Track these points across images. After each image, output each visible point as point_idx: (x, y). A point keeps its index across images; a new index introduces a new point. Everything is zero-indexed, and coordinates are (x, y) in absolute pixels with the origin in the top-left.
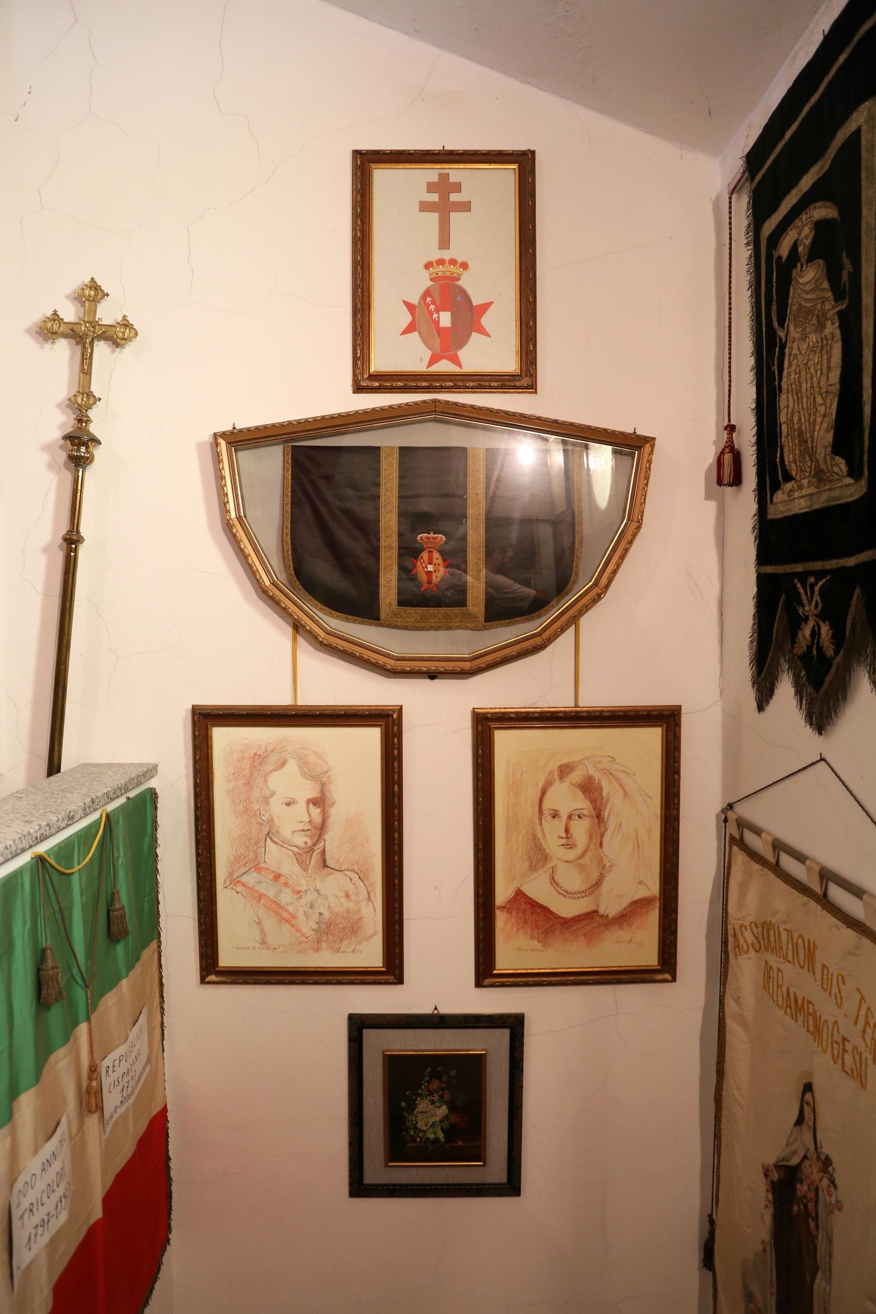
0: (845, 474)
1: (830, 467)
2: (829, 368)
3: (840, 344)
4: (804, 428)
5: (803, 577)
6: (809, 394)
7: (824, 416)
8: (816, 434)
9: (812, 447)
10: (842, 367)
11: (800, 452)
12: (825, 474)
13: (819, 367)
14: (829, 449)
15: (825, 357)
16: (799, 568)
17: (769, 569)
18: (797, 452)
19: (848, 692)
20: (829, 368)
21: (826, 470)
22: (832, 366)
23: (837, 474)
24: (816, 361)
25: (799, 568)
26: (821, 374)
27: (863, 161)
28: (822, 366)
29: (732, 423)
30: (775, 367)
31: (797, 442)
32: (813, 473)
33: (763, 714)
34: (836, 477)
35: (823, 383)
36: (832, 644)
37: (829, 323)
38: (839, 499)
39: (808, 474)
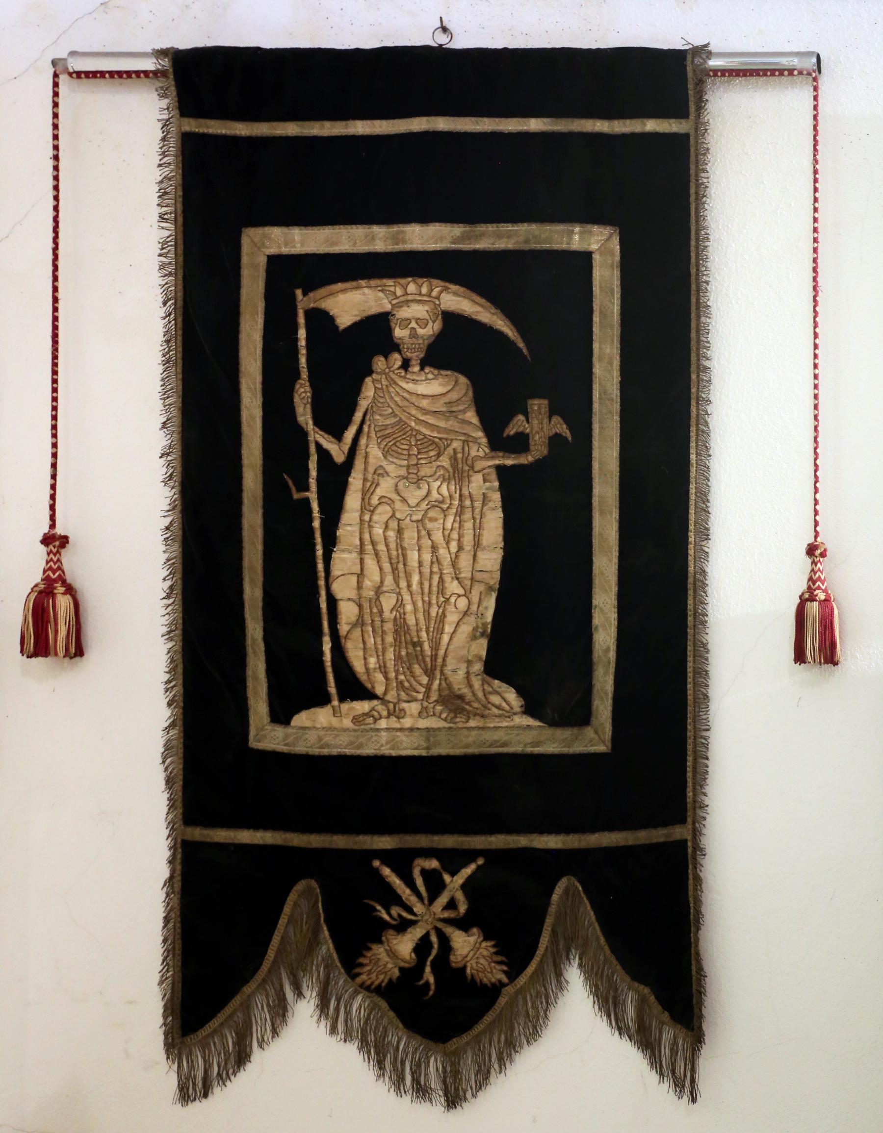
0: (518, 710)
1: (480, 695)
2: (477, 544)
3: (499, 514)
4: (411, 620)
5: (391, 858)
6: (426, 570)
7: (466, 613)
8: (446, 638)
9: (434, 657)
10: (505, 549)
11: (398, 657)
12: (469, 704)
13: (455, 535)
14: (478, 667)
15: (469, 525)
16: (385, 842)
17: (197, 834)
18: (390, 655)
19: (705, 1027)
20: (477, 544)
21: (469, 696)
22: (484, 542)
23: (498, 707)
24: (449, 525)
25: (385, 842)
26: (460, 548)
27: (596, 307)
28: (460, 536)
29: (59, 530)
30: (313, 495)
31: (389, 639)
32: (434, 697)
33: (198, 1108)
34: (496, 711)
35: (465, 562)
36: (390, 980)
37: (477, 478)
38: (504, 745)
39: (420, 696)
